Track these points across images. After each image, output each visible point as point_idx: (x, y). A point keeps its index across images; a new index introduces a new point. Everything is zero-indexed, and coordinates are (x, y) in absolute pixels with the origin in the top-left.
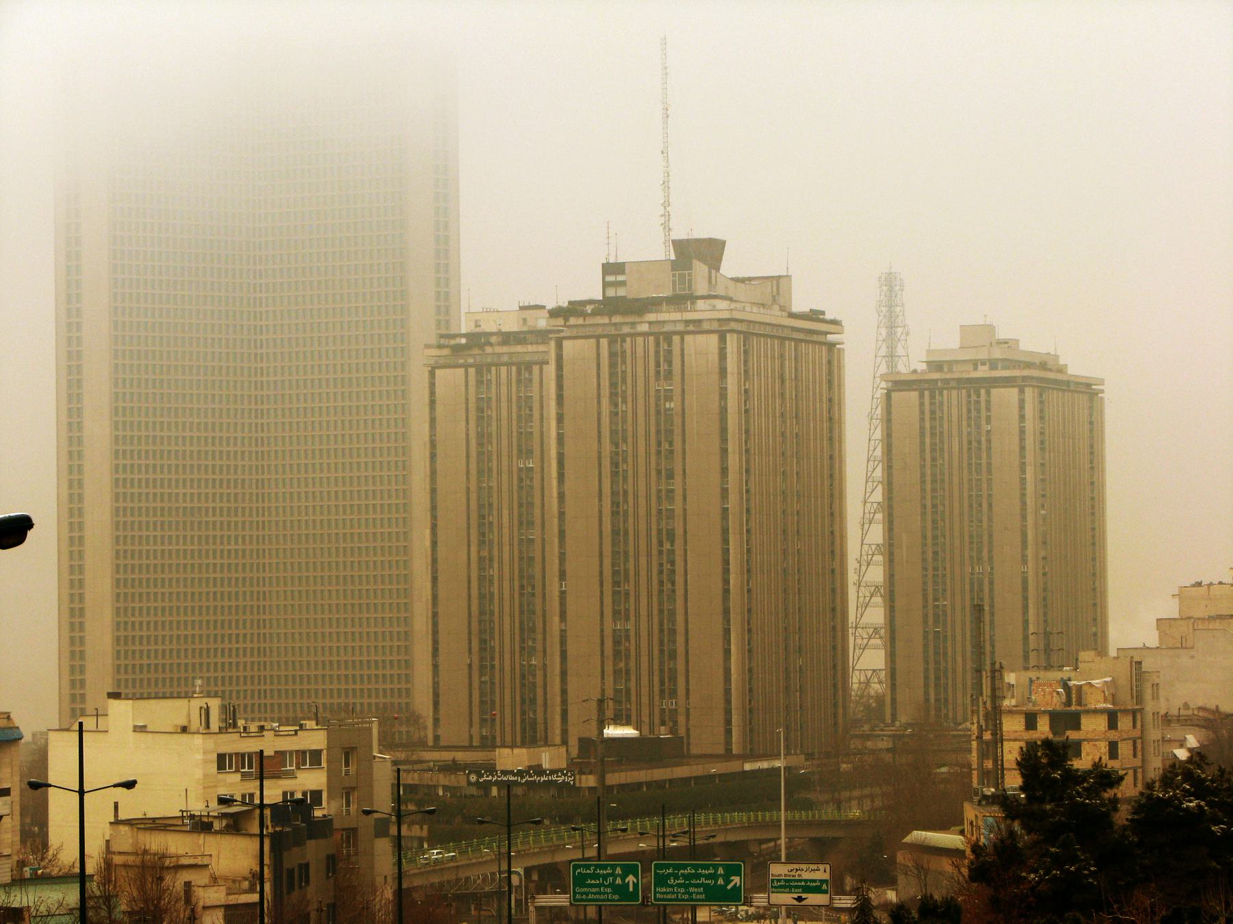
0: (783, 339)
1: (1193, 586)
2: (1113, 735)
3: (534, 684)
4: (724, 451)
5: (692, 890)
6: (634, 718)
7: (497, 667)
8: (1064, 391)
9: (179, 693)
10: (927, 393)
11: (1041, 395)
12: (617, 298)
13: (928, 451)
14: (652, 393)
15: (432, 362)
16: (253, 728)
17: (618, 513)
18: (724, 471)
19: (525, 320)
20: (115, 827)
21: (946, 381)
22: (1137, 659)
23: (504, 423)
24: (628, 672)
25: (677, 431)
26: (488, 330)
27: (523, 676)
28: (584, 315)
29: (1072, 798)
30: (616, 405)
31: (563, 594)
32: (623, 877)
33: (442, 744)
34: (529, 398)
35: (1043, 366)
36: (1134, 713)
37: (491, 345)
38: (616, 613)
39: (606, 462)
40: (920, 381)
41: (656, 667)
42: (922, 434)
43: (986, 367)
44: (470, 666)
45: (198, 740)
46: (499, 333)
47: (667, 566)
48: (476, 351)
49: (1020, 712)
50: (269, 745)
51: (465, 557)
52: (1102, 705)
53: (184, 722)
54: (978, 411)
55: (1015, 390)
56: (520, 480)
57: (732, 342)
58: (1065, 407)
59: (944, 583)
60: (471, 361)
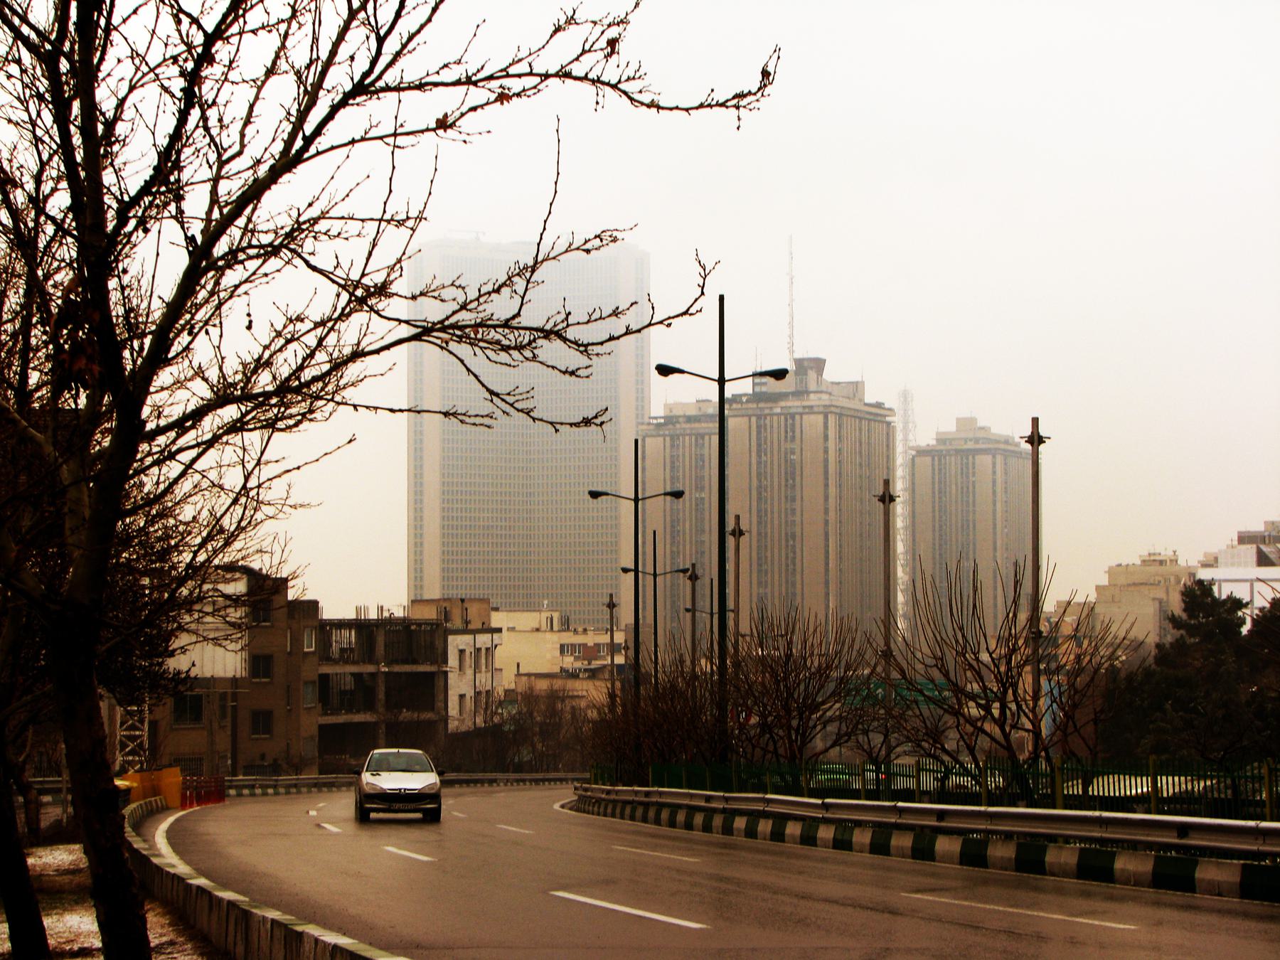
0: (861, 419)
16: (580, 629)
18: (826, 498)
21: (948, 451)
25: (798, 472)
34: (702, 455)
35: (1007, 442)
38: (760, 583)
42: (933, 483)
45: (549, 635)
46: (684, 416)
47: (791, 555)
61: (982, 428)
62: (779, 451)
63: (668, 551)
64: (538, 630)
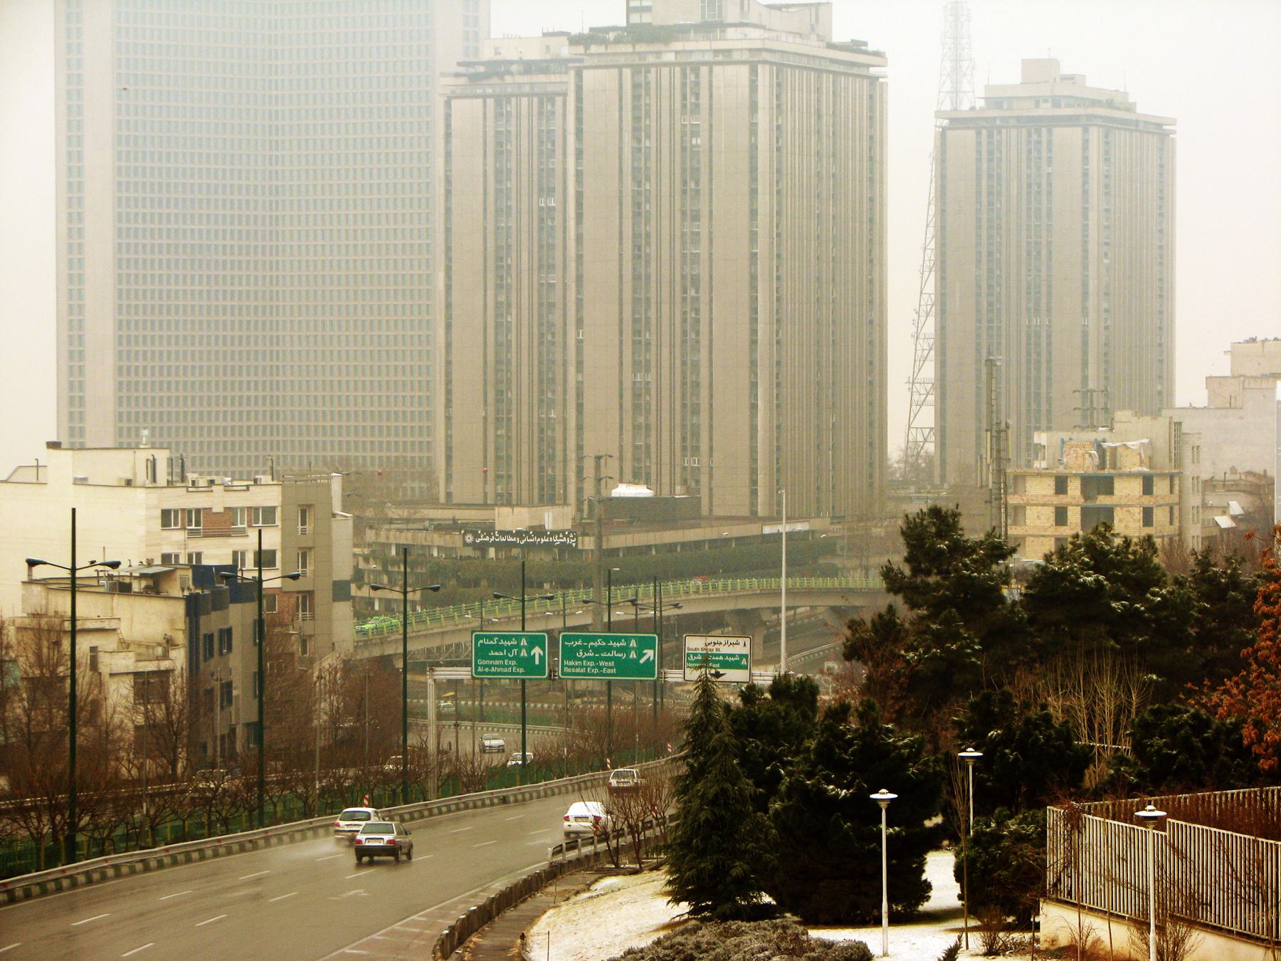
0: (820, 72)
1: (1247, 342)
2: (1147, 501)
3: (553, 439)
4: (753, 192)
5: (602, 663)
6: (653, 477)
7: (514, 420)
8: (1131, 131)
9: (162, 443)
10: (984, 132)
11: (1107, 137)
12: (641, 25)
13: (984, 194)
14: (678, 127)
15: (448, 92)
16: (202, 482)
17: (640, 257)
18: (753, 213)
19: (548, 47)
20: (29, 586)
21: (1004, 119)
22: (1176, 420)
23: (524, 158)
24: (648, 427)
26: (508, 58)
27: (542, 431)
28: (605, 42)
29: (956, 570)
30: (639, 141)
31: (579, 342)
32: (529, 649)
33: (455, 501)
34: (550, 132)
35: (1110, 104)
36: (1172, 477)
37: (511, 74)
38: (636, 364)
39: (628, 202)
40: (978, 118)
41: (678, 421)
42: (979, 177)
43: (1049, 105)
44: (485, 418)
45: (140, 494)
46: (521, 62)
48: (495, 80)
49: (1050, 475)
50: (217, 501)
51: (481, 303)
52: (1136, 469)
53: (130, 476)
54: (1039, 151)
55: (1079, 130)
56: (541, 220)
57: (764, 74)
58: (1135, 148)
59: (999, 336)
60: (489, 91)
61: (1070, 78)
62: (672, 127)
63: (491, 304)
64: (129, 483)
